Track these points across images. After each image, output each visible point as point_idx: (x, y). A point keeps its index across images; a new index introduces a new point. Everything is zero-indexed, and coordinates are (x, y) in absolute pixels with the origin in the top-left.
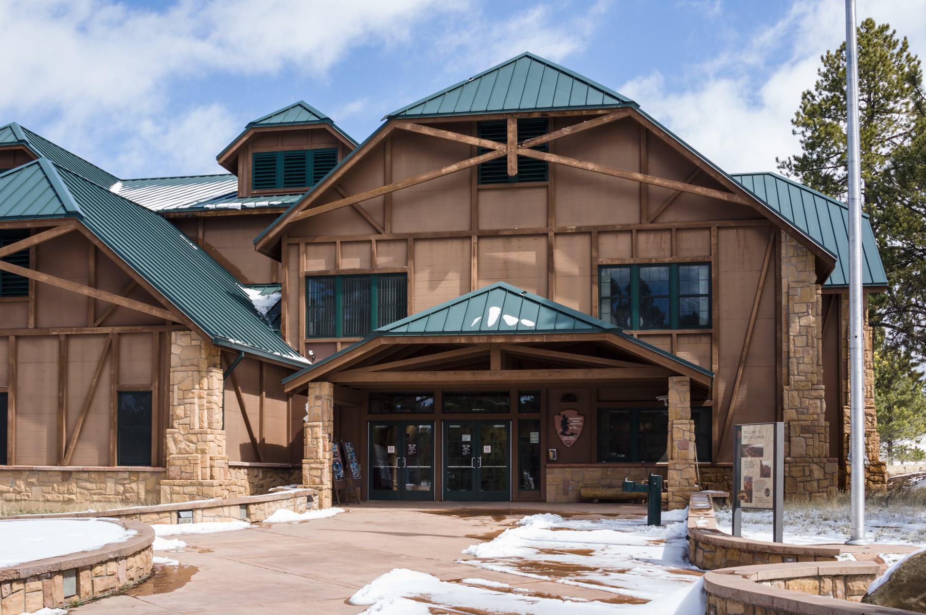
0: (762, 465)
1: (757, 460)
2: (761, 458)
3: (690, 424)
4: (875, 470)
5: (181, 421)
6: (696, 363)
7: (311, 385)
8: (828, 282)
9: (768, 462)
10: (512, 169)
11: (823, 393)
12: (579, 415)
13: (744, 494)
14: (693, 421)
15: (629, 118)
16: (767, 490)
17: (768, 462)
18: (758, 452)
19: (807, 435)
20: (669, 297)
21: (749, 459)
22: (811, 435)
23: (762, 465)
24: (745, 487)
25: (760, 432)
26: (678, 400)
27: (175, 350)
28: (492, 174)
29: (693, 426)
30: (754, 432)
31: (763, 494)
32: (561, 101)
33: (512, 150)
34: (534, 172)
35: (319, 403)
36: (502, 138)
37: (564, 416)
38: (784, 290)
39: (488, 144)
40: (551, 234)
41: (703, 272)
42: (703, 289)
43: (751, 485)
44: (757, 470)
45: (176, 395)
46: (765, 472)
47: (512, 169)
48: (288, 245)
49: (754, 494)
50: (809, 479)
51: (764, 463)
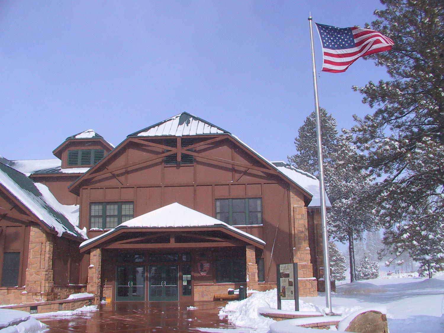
0: (289, 281)
1: (287, 279)
2: (289, 278)
3: (256, 265)
4: (333, 284)
5: (33, 266)
6: (235, 246)
7: (91, 249)
8: (309, 206)
9: (292, 280)
10: (179, 159)
11: (309, 252)
12: (208, 262)
13: (282, 294)
14: (257, 264)
15: (227, 139)
16: (292, 291)
17: (292, 280)
18: (287, 276)
19: (303, 269)
20: (233, 213)
21: (284, 278)
22: (305, 269)
23: (289, 281)
24: (282, 291)
25: (287, 267)
26: (250, 254)
27: (32, 233)
28: (171, 159)
29: (257, 266)
30: (285, 267)
31: (290, 293)
32: (200, 132)
33: (179, 151)
34: (187, 159)
35: (95, 257)
36: (175, 146)
37: (201, 263)
38: (292, 209)
39: (169, 148)
40: (195, 186)
41: (259, 202)
42: (259, 209)
43: (285, 290)
44: (287, 283)
45: (31, 253)
46: (290, 284)
47: (179, 159)
48: (83, 189)
49: (286, 293)
50: (305, 288)
51: (290, 280)
